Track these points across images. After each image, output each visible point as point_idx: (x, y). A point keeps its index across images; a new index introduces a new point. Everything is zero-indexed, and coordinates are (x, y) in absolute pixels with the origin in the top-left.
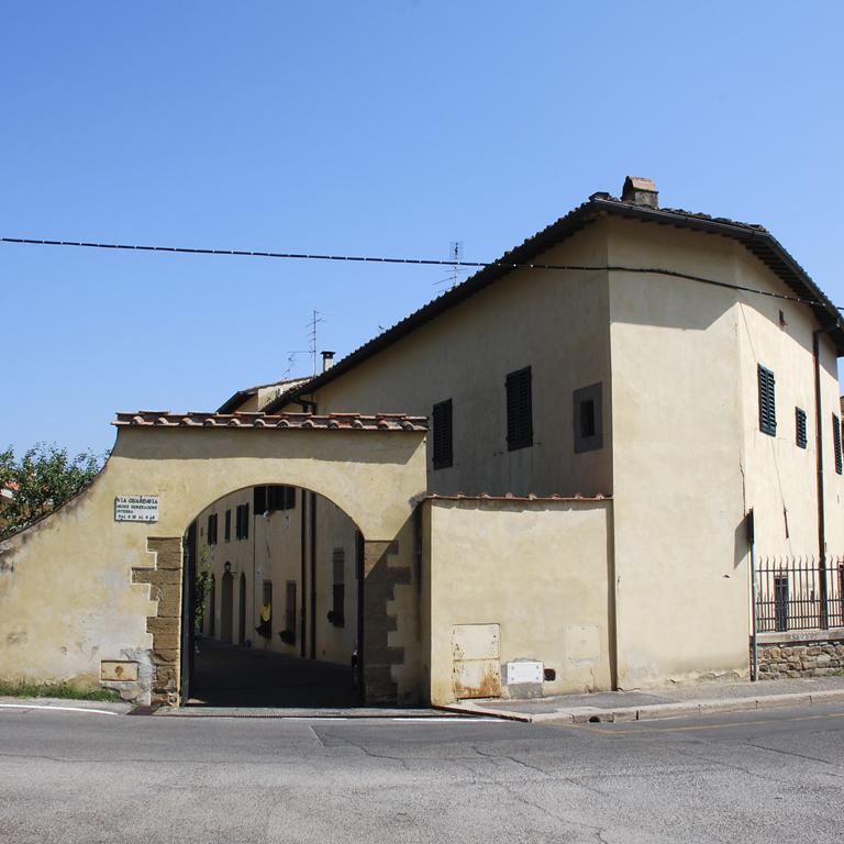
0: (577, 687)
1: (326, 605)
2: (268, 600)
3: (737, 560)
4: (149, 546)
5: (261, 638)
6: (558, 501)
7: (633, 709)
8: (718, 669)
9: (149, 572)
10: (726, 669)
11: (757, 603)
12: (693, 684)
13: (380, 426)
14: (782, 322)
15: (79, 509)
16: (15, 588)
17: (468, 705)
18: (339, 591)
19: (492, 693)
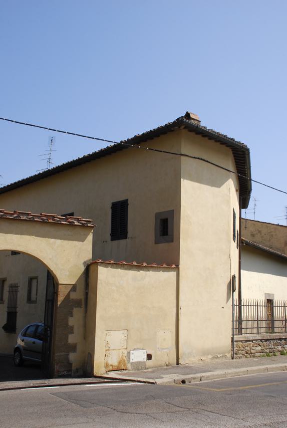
7: (199, 375)
8: (219, 354)
12: (210, 361)
19: (123, 368)
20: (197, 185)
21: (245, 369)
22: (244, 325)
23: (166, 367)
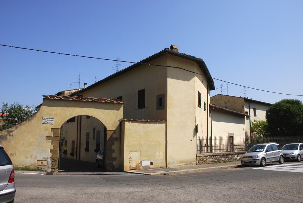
0: (157, 167)
1: (83, 146)
2: (66, 145)
3: (194, 137)
4: (51, 130)
5: (64, 154)
6: (160, 122)
7: (173, 172)
8: (189, 162)
9: (51, 137)
10: (191, 162)
11: (197, 147)
12: (184, 166)
13: (112, 102)
14: (202, 82)
15: (32, 120)
16: (13, 141)
17: (133, 171)
18: (87, 143)
20: (176, 80)
21: (199, 169)
22: (213, 148)
23: (160, 168)
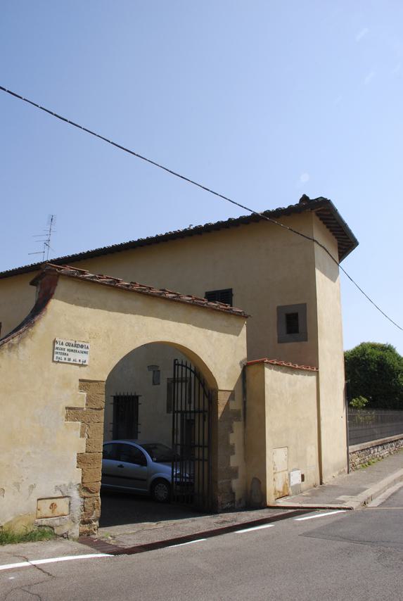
19: (287, 494)
